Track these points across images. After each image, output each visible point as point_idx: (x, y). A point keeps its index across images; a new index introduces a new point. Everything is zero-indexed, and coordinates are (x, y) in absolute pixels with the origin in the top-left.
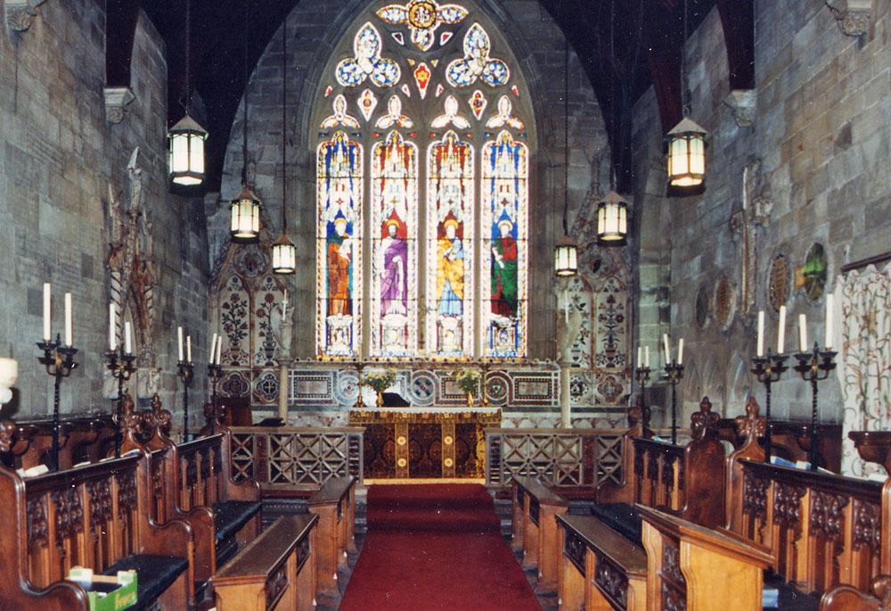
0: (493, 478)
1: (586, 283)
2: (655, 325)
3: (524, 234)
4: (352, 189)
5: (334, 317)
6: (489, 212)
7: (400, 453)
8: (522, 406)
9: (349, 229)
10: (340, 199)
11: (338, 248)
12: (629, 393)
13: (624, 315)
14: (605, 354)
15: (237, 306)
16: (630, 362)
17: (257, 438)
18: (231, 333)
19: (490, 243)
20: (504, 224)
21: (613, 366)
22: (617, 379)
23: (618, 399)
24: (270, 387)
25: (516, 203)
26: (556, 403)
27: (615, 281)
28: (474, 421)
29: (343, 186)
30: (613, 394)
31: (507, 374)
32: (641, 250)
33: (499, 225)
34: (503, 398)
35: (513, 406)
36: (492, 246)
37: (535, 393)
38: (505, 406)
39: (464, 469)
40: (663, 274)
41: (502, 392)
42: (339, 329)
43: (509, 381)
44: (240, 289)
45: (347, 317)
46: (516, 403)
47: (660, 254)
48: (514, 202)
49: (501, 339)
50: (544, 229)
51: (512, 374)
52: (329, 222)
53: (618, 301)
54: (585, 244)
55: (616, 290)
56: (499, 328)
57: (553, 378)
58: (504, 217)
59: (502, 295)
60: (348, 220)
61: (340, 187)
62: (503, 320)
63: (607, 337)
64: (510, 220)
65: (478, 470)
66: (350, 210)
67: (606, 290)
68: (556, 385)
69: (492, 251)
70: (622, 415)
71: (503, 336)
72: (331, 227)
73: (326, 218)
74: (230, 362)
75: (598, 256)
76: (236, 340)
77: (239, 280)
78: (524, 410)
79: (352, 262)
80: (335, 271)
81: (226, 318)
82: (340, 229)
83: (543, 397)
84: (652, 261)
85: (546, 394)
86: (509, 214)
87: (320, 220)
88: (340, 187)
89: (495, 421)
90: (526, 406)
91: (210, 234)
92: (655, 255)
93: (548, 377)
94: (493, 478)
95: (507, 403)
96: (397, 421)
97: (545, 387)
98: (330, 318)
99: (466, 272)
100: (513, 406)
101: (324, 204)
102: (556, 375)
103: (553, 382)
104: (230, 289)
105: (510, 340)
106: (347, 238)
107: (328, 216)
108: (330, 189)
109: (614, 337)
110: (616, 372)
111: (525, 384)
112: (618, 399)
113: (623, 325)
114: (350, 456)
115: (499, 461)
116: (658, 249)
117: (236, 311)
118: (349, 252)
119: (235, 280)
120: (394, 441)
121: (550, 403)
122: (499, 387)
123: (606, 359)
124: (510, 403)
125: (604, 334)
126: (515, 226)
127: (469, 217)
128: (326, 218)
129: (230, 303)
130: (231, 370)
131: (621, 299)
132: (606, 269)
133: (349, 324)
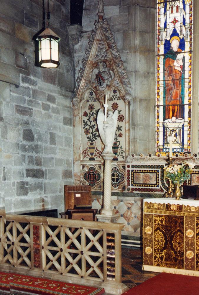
4: (184, 9)
5: (170, 120)
7: (188, 245)
9: (182, 46)
10: (175, 19)
11: (173, 62)
15: (92, 115)
17: (34, 226)
18: (89, 136)
24: (115, 177)
29: (178, 7)
42: (173, 131)
44: (95, 101)
45: (180, 120)
52: (166, 40)
57: (131, 169)
60: (181, 37)
61: (175, 9)
66: (183, 28)
72: (167, 44)
73: (164, 38)
74: (89, 157)
76: (92, 141)
77: (94, 93)
79: (184, 73)
80: (170, 82)
81: (86, 124)
82: (175, 45)
86: (178, 31)
87: (159, 39)
88: (175, 9)
91: (76, 59)
96: (186, 214)
98: (166, 121)
101: (162, 25)
102: (128, 166)
104: (88, 101)
106: (180, 52)
107: (165, 36)
108: (168, 12)
114: (108, 253)
117: (92, 118)
118: (182, 64)
119: (91, 94)
120: (183, 233)
128: (164, 38)
129: (88, 111)
130: (88, 164)
133: (181, 126)
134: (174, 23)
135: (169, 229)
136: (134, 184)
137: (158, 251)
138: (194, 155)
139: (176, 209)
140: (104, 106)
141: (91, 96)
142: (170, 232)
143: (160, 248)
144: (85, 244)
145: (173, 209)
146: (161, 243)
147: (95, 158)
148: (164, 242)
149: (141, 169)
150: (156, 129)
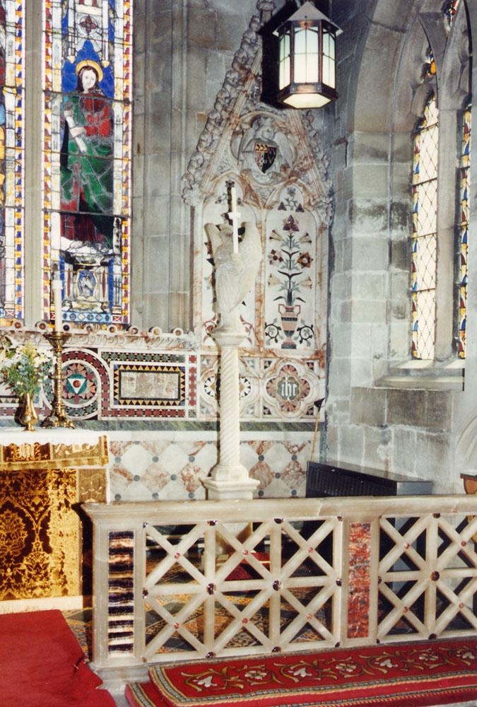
0: (116, 642)
1: (248, 190)
2: (382, 272)
3: (126, 91)
6: (57, 41)
8: (127, 418)
12: (322, 395)
13: (312, 256)
14: (279, 323)
16: (324, 340)
19: (57, 103)
20: (87, 68)
21: (294, 347)
22: (302, 370)
23: (303, 405)
25: (111, 29)
26: (193, 413)
27: (298, 190)
28: (44, 464)
30: (292, 398)
31: (98, 356)
32: (356, 133)
33: (79, 67)
34: (90, 402)
35: (110, 419)
36: (64, 107)
37: (152, 395)
38: (95, 418)
39: (18, 577)
40: (396, 179)
41: (87, 391)
43: (102, 371)
46: (116, 413)
47: (393, 143)
48: (106, 26)
49: (81, 288)
50: (168, 83)
51: (109, 356)
53: (303, 227)
54: (248, 118)
55: (300, 209)
56: (76, 267)
57: (187, 365)
58: (88, 52)
59: (84, 205)
62: (84, 251)
63: (284, 293)
64: (99, 61)
65: (52, 577)
67: (282, 207)
68: (192, 379)
69: (62, 117)
70: (309, 435)
71: (85, 282)
75: (270, 142)
78: (132, 426)
83: (168, 401)
84: (378, 154)
85: (174, 395)
86: (96, 48)
89: (91, 462)
90: (135, 418)
92: (381, 143)
93: (177, 364)
94: (116, 642)
95: (98, 412)
97: (171, 383)
99: (11, 153)
100: (110, 419)
102: (193, 359)
103: (188, 375)
105: (98, 290)
109: (295, 294)
110: (299, 357)
111: (134, 375)
112: (303, 405)
113: (311, 271)
115: (129, 596)
116: (389, 133)
121: (181, 413)
122: (82, 381)
123: (282, 333)
124: (105, 413)
125: (279, 286)
126: (109, 73)
127: (16, 45)
131: (309, 223)
132: (285, 168)
134: (86, 22)
135: (37, 503)
136: (123, 399)
137: (6, 562)
138: (38, 324)
139: (33, 454)
140: (230, 218)
141: (290, 198)
142: (41, 509)
143: (15, 553)
144: (442, 528)
145: (25, 456)
146: (17, 540)
147: (296, 343)
148: (24, 537)
149: (144, 363)
150: (43, 266)
